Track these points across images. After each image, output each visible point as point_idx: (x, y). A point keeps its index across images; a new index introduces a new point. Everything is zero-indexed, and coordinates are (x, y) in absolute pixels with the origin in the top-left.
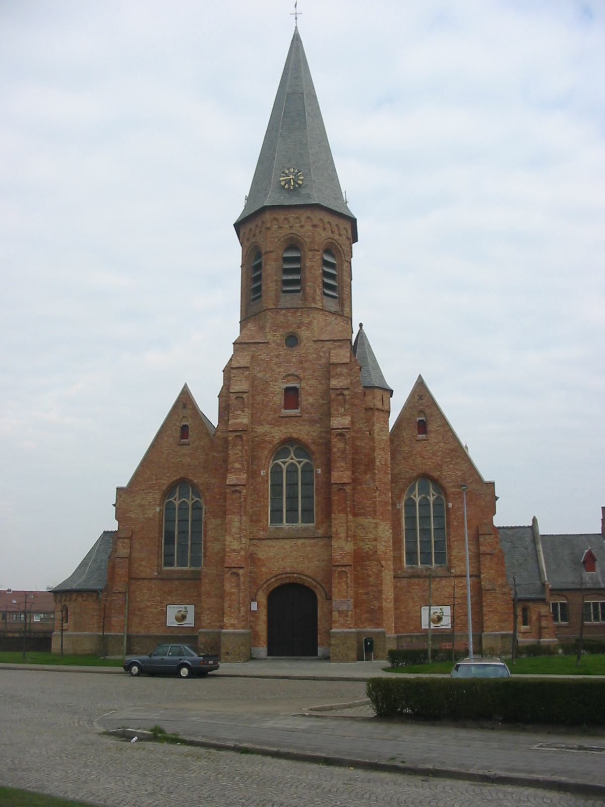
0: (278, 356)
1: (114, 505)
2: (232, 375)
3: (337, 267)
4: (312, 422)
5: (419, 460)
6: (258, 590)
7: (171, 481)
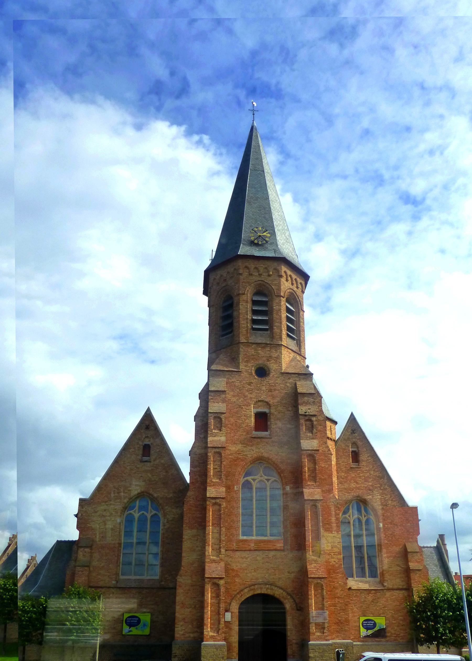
0: (250, 384)
1: (76, 516)
2: (210, 397)
3: (295, 314)
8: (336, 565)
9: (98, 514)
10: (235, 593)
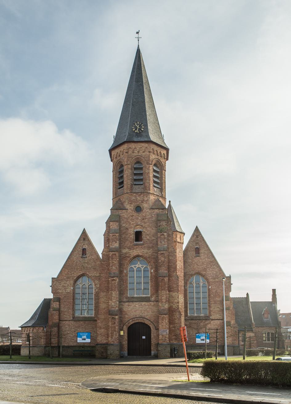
0: (132, 216)
1: (51, 286)
2: (111, 225)
3: (160, 173)
4: (149, 248)
5: (196, 266)
6: (123, 326)
7: (78, 275)
8: (176, 308)
9: (61, 285)
10: (125, 322)
